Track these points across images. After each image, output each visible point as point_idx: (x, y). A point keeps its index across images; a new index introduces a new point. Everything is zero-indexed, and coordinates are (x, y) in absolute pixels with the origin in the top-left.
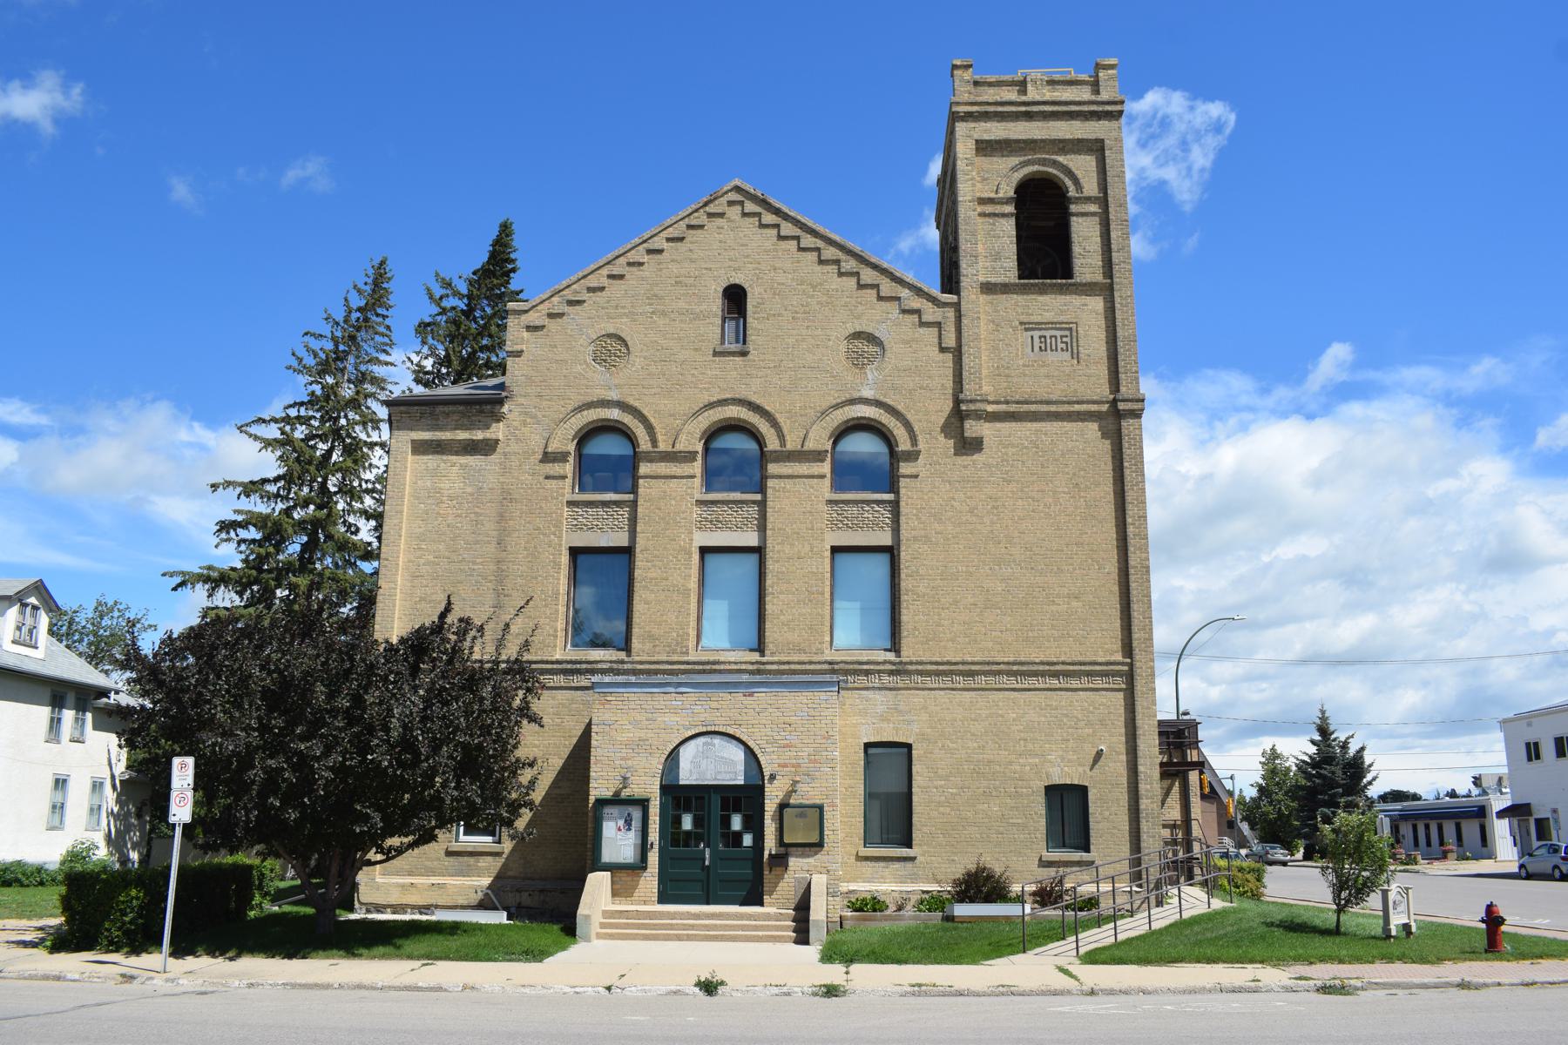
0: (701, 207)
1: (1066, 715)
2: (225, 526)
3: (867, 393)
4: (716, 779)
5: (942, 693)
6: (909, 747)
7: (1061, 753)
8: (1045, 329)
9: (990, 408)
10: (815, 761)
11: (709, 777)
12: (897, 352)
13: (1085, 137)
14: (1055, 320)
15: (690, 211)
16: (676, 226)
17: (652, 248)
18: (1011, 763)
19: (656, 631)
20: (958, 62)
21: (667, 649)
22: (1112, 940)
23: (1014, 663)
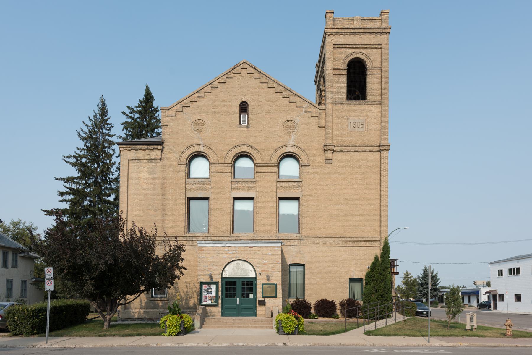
2: (62, 194)
3: (291, 143)
6: (304, 265)
7: (355, 268)
11: (238, 275)
16: (222, 78)
19: (219, 227)
22: (375, 329)
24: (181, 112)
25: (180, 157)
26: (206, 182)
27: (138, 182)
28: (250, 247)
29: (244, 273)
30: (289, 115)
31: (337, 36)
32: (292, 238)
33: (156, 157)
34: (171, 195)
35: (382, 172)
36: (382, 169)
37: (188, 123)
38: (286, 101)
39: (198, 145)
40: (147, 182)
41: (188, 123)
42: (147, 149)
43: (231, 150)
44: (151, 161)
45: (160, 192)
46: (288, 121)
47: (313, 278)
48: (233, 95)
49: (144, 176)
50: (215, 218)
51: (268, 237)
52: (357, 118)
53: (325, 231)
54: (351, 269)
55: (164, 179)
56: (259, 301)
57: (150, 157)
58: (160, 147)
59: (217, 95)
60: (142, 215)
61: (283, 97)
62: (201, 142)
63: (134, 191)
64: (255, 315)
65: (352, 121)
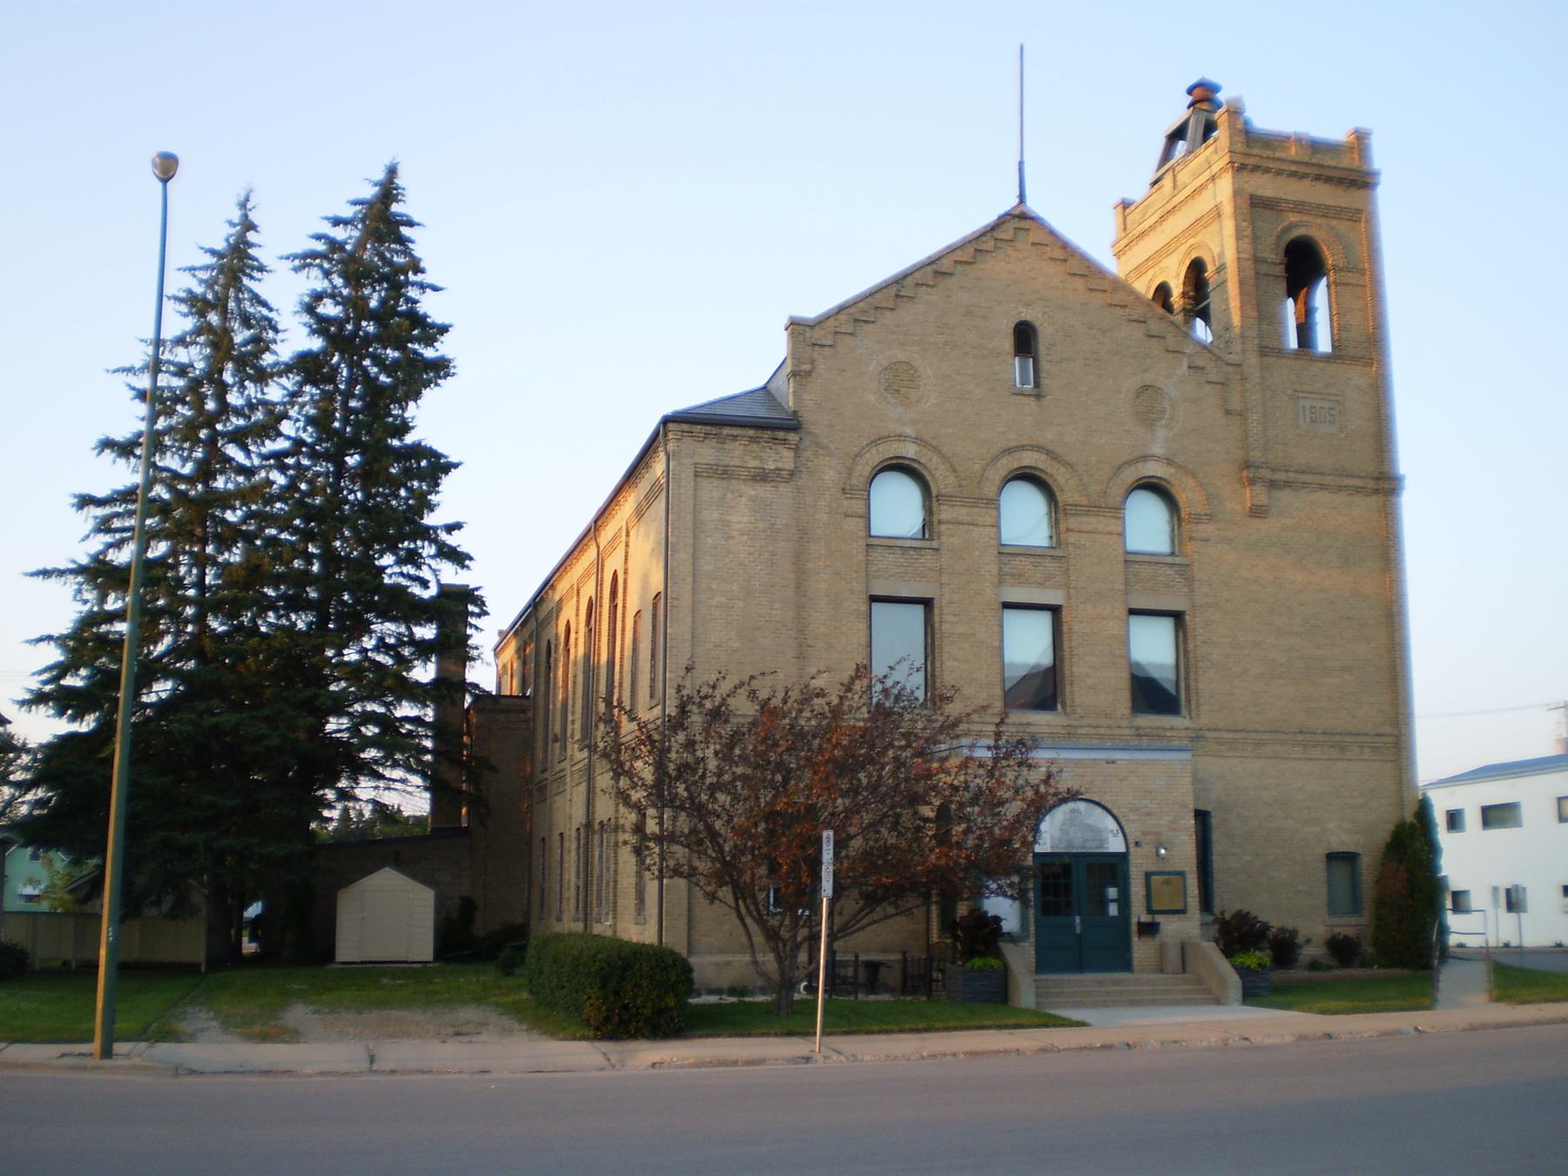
4: (1084, 847)
10: (1174, 829)
17: (940, 270)
24: (848, 337)
25: (850, 471)
26: (923, 552)
27: (723, 542)
28: (1108, 763)
29: (1093, 840)
30: (1146, 371)
31: (1257, 175)
32: (1174, 733)
33: (780, 465)
34: (823, 586)
37: (871, 369)
38: (1138, 332)
39: (901, 437)
40: (749, 543)
41: (871, 369)
42: (752, 440)
43: (995, 459)
44: (762, 477)
45: (792, 576)
46: (1146, 387)
47: (1233, 855)
49: (739, 523)
50: (955, 664)
51: (1109, 727)
52: (1319, 396)
54: (1331, 826)
55: (803, 536)
56: (1139, 924)
57: (761, 465)
58: (792, 437)
59: (949, 297)
60: (736, 645)
61: (1130, 321)
62: (908, 431)
63: (710, 568)
64: (1127, 966)
65: (1307, 404)
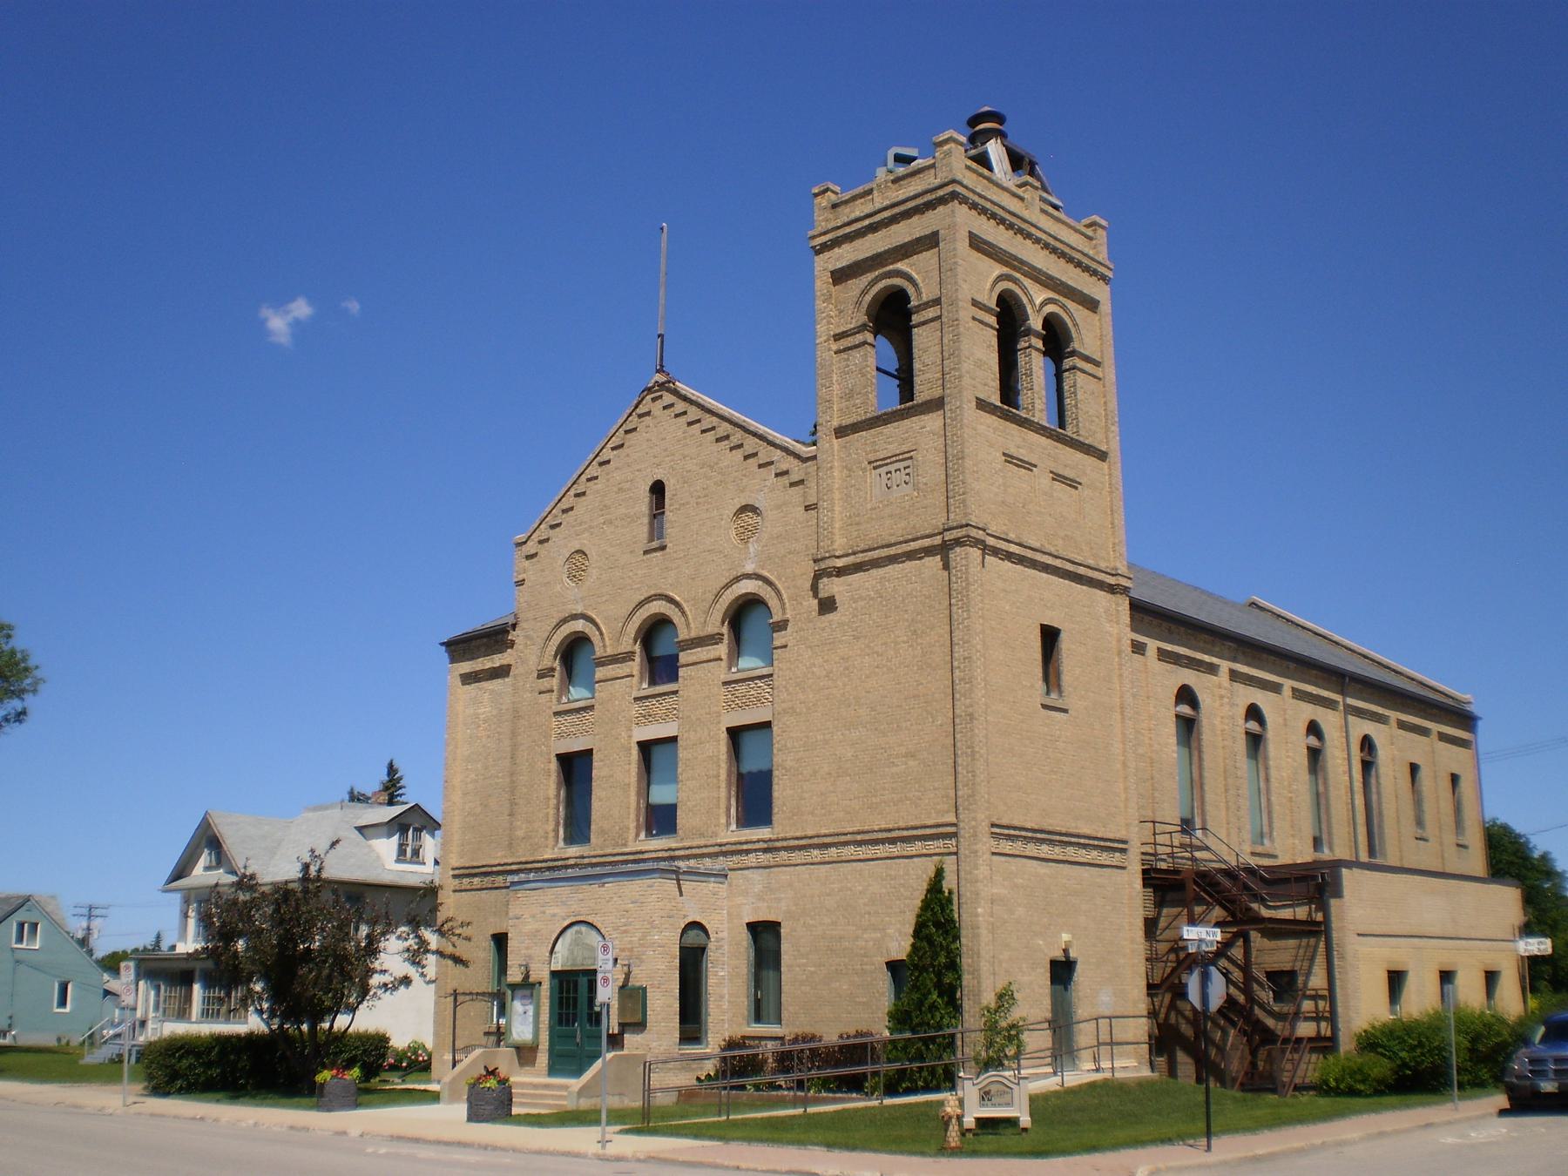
0: (633, 411)
1: (903, 885)
3: (749, 568)
5: (803, 868)
7: (898, 926)
8: (887, 464)
9: (840, 563)
11: (579, 962)
12: (771, 523)
13: (922, 234)
14: (898, 452)
15: (626, 416)
17: (602, 460)
18: (857, 938)
20: (816, 190)
21: (613, 842)
23: (859, 833)
35: (954, 609)
36: (953, 601)
43: (631, 614)
48: (638, 471)
53: (825, 815)
